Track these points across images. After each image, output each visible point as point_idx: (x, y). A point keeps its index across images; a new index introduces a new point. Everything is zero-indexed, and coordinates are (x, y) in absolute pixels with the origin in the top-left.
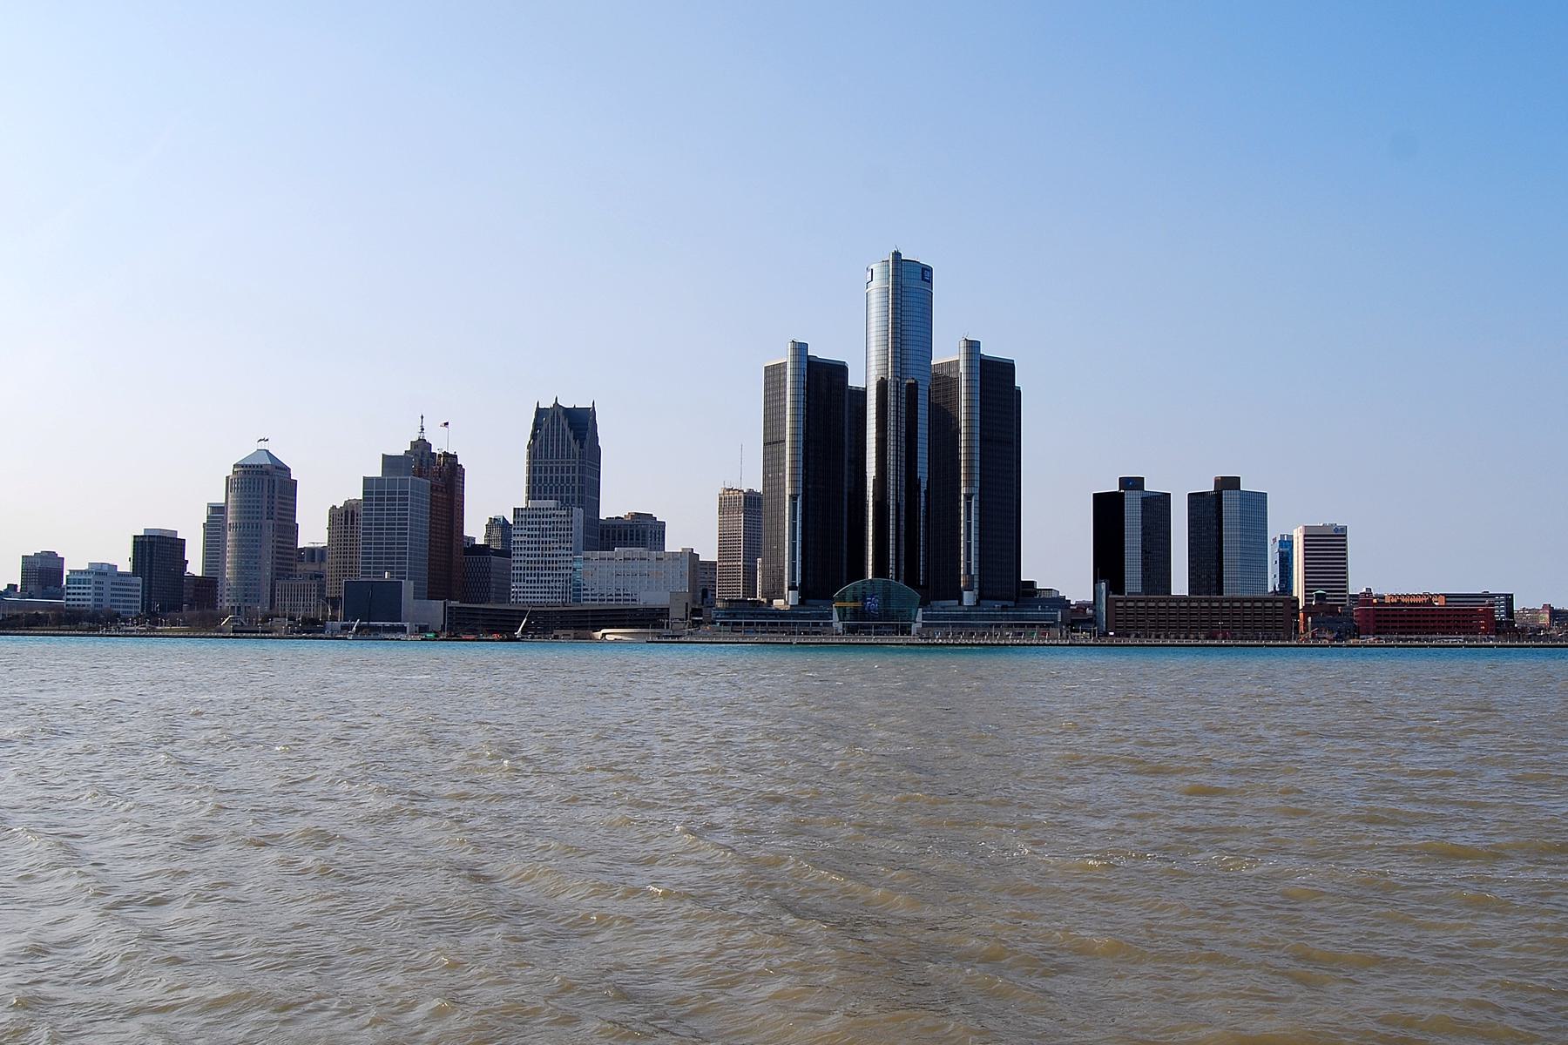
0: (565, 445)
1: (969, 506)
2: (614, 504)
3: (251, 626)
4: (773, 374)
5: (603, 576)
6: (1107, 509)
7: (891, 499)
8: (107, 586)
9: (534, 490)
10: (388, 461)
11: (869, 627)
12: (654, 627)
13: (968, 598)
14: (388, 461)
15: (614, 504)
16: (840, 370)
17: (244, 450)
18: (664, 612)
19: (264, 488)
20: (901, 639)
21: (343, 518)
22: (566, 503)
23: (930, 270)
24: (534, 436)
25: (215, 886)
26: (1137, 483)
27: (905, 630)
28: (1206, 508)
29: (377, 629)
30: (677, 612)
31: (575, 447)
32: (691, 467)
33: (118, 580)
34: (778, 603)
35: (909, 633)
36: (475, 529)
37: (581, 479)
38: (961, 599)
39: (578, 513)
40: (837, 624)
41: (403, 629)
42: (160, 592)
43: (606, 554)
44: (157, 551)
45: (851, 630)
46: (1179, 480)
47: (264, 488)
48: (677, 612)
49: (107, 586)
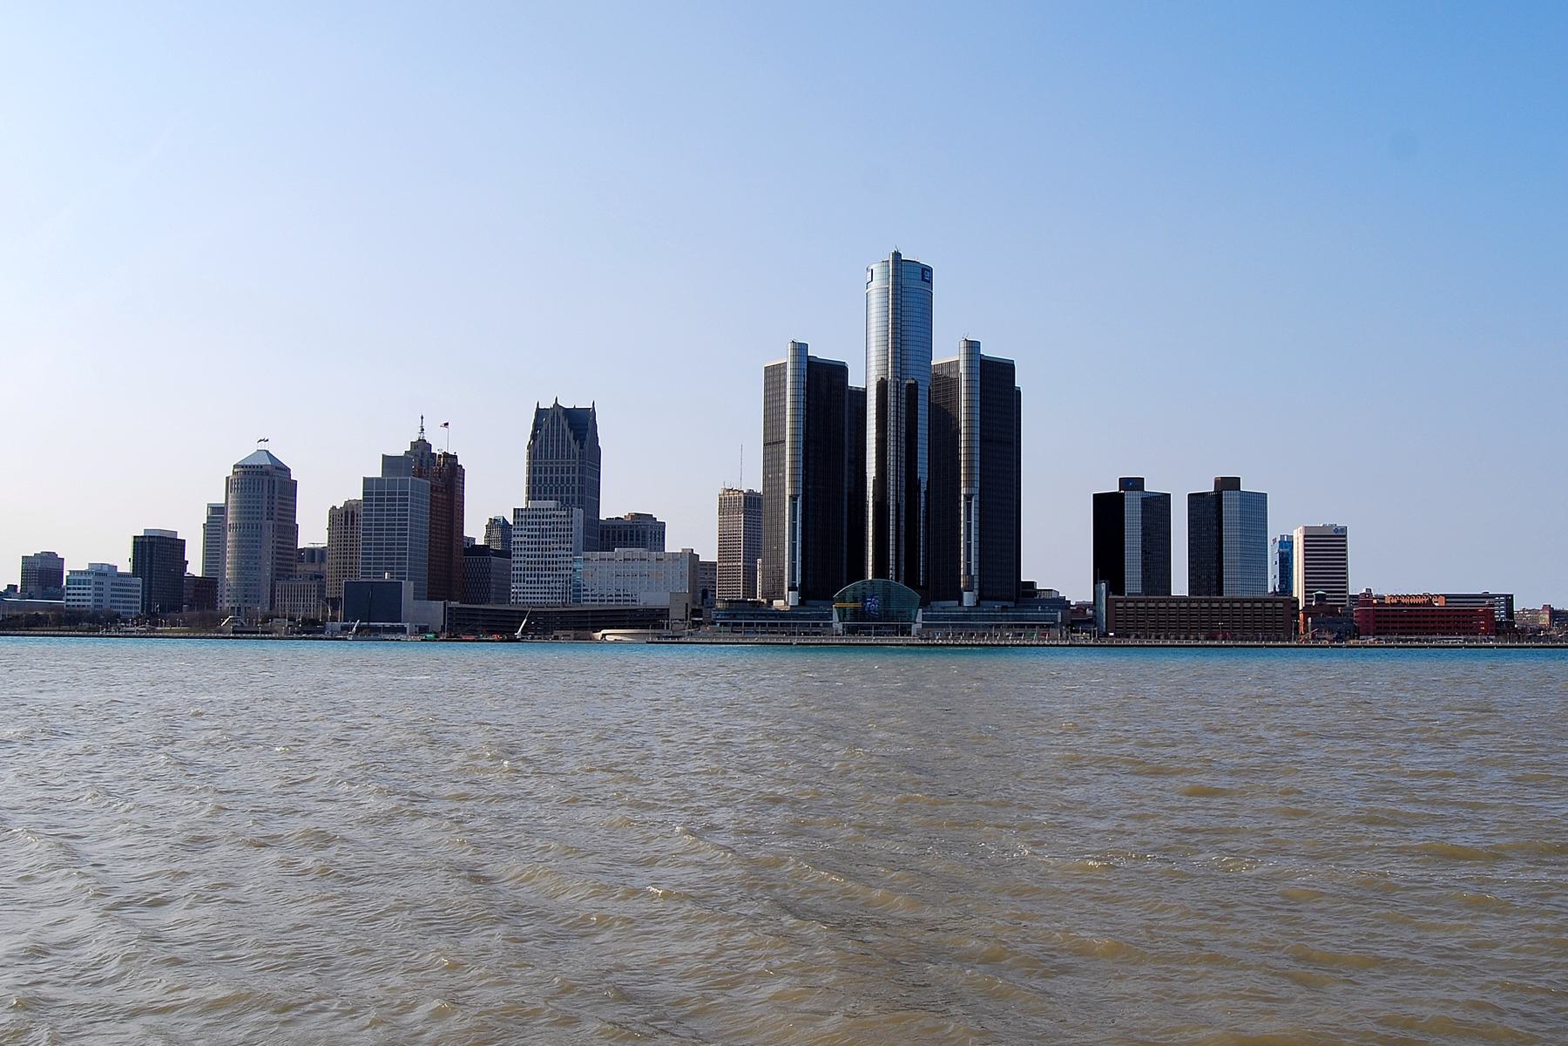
0: (565, 445)
1: (969, 506)
2: (614, 505)
3: (251, 627)
4: (773, 375)
5: (603, 576)
6: (1107, 510)
7: (891, 499)
8: (107, 587)
9: (534, 491)
10: (388, 461)
11: (869, 627)
12: (654, 627)
13: (968, 599)
14: (388, 461)
15: (614, 505)
16: (840, 370)
17: (244, 451)
18: (664, 613)
19: (264, 488)
20: (901, 639)
21: (343, 518)
22: (566, 504)
24: (534, 436)
25: (215, 887)
26: (1137, 484)
27: (905, 631)
28: (1206, 508)
29: (377, 630)
30: (677, 613)
31: (575, 447)
32: (691, 467)
33: (118, 580)
34: (778, 604)
35: (909, 634)
36: (475, 529)
37: (581, 480)
38: (961, 600)
39: (578, 513)
40: (837, 625)
41: (403, 630)
42: (160, 592)
43: (606, 554)
44: (157, 551)
45: (851, 631)
46: (1179, 480)
47: (264, 488)
48: (677, 613)
49: (107, 587)
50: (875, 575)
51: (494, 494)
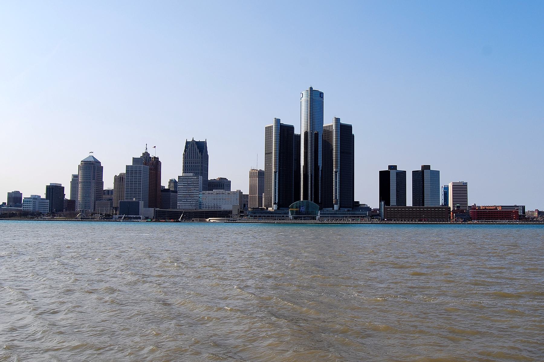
0: (196, 154)
1: (336, 175)
2: (213, 175)
3: (87, 217)
4: (268, 130)
5: (209, 200)
6: (384, 176)
7: (309, 173)
8: (37, 203)
9: (185, 170)
10: (135, 160)
11: (301, 217)
12: (227, 217)
13: (336, 207)
14: (135, 160)
15: (213, 175)
16: (291, 128)
17: (85, 156)
18: (230, 212)
19: (92, 169)
20: (312, 221)
21: (119, 179)
22: (196, 174)
23: (323, 93)
24: (185, 151)
26: (394, 167)
27: (314, 218)
28: (419, 176)
29: (131, 218)
30: (235, 212)
31: (200, 155)
32: (240, 162)
33: (41, 201)
34: (270, 209)
35: (315, 219)
36: (165, 183)
37: (202, 166)
38: (333, 208)
39: (201, 178)
40: (291, 216)
41: (140, 218)
42: (56, 205)
43: (210, 192)
44: (55, 191)
45: (295, 218)
46: (409, 166)
47: (92, 169)
48: (235, 212)
49: (37, 203)
50: (303, 199)
51: (171, 171)
